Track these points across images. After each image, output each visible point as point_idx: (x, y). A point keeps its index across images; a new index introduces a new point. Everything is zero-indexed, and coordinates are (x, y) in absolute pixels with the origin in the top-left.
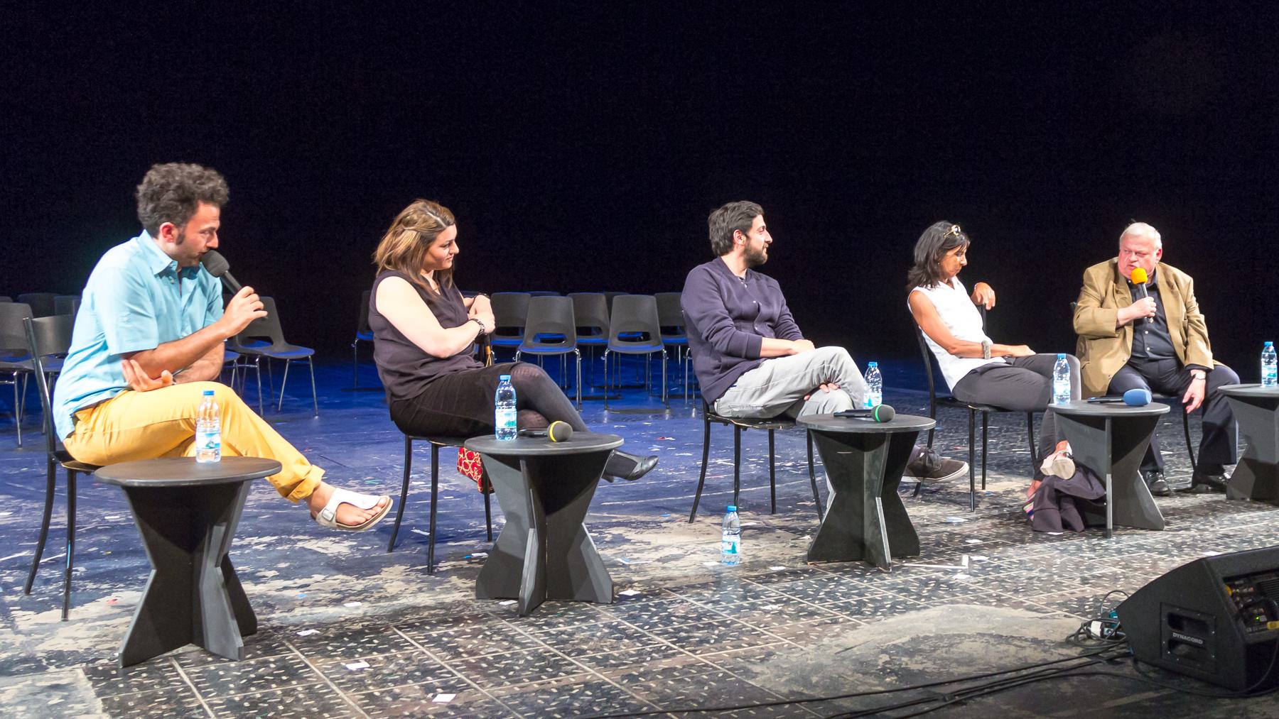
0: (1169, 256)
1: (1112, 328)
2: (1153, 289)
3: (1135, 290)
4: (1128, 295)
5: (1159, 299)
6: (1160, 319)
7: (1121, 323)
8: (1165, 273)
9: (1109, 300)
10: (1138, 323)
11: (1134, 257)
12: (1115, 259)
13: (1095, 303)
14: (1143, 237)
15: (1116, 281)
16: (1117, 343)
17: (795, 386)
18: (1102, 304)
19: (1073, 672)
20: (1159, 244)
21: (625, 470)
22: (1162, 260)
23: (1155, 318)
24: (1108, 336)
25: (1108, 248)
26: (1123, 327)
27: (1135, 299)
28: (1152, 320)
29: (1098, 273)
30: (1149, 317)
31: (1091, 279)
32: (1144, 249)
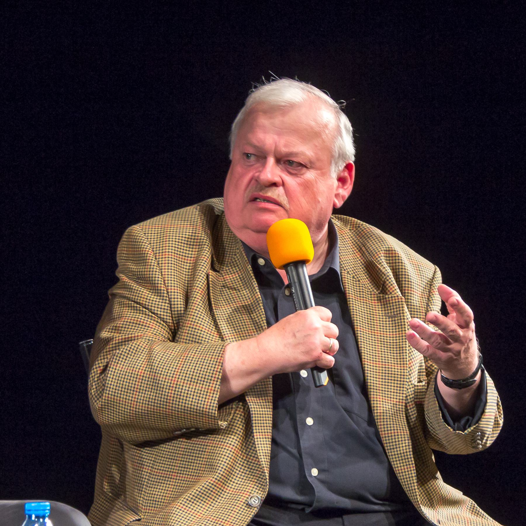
0: (377, 195)
1: (206, 399)
2: (329, 287)
3: (274, 289)
4: (253, 294)
5: (344, 317)
6: (347, 375)
7: (237, 385)
8: (362, 246)
9: (199, 318)
10: (282, 386)
11: (271, 171)
12: (216, 202)
13: (156, 330)
14: (304, 122)
15: (218, 259)
16: (229, 446)
17: (200, 425)
18: (174, 335)
19: (293, 506)
20: (347, 145)
21: (454, 354)
22: (352, 208)
23: (333, 373)
24: (196, 430)
25: (193, 165)
26: (241, 398)
27: (275, 315)
28: (324, 378)
29: (165, 244)
30: (316, 368)
31: (140, 258)
32: (305, 150)
